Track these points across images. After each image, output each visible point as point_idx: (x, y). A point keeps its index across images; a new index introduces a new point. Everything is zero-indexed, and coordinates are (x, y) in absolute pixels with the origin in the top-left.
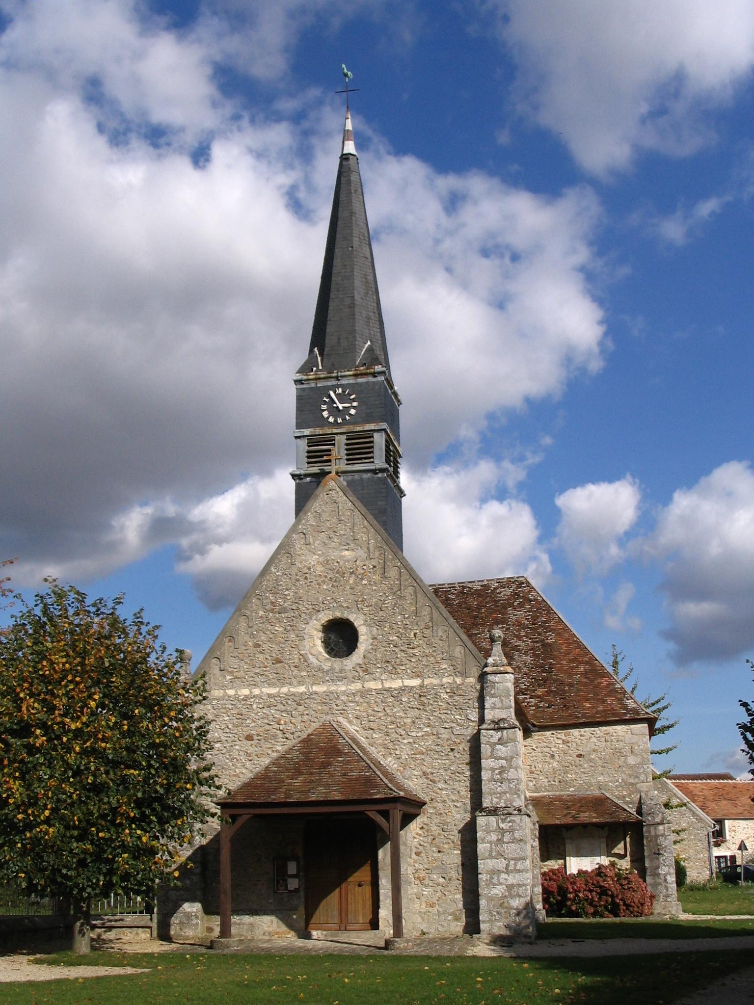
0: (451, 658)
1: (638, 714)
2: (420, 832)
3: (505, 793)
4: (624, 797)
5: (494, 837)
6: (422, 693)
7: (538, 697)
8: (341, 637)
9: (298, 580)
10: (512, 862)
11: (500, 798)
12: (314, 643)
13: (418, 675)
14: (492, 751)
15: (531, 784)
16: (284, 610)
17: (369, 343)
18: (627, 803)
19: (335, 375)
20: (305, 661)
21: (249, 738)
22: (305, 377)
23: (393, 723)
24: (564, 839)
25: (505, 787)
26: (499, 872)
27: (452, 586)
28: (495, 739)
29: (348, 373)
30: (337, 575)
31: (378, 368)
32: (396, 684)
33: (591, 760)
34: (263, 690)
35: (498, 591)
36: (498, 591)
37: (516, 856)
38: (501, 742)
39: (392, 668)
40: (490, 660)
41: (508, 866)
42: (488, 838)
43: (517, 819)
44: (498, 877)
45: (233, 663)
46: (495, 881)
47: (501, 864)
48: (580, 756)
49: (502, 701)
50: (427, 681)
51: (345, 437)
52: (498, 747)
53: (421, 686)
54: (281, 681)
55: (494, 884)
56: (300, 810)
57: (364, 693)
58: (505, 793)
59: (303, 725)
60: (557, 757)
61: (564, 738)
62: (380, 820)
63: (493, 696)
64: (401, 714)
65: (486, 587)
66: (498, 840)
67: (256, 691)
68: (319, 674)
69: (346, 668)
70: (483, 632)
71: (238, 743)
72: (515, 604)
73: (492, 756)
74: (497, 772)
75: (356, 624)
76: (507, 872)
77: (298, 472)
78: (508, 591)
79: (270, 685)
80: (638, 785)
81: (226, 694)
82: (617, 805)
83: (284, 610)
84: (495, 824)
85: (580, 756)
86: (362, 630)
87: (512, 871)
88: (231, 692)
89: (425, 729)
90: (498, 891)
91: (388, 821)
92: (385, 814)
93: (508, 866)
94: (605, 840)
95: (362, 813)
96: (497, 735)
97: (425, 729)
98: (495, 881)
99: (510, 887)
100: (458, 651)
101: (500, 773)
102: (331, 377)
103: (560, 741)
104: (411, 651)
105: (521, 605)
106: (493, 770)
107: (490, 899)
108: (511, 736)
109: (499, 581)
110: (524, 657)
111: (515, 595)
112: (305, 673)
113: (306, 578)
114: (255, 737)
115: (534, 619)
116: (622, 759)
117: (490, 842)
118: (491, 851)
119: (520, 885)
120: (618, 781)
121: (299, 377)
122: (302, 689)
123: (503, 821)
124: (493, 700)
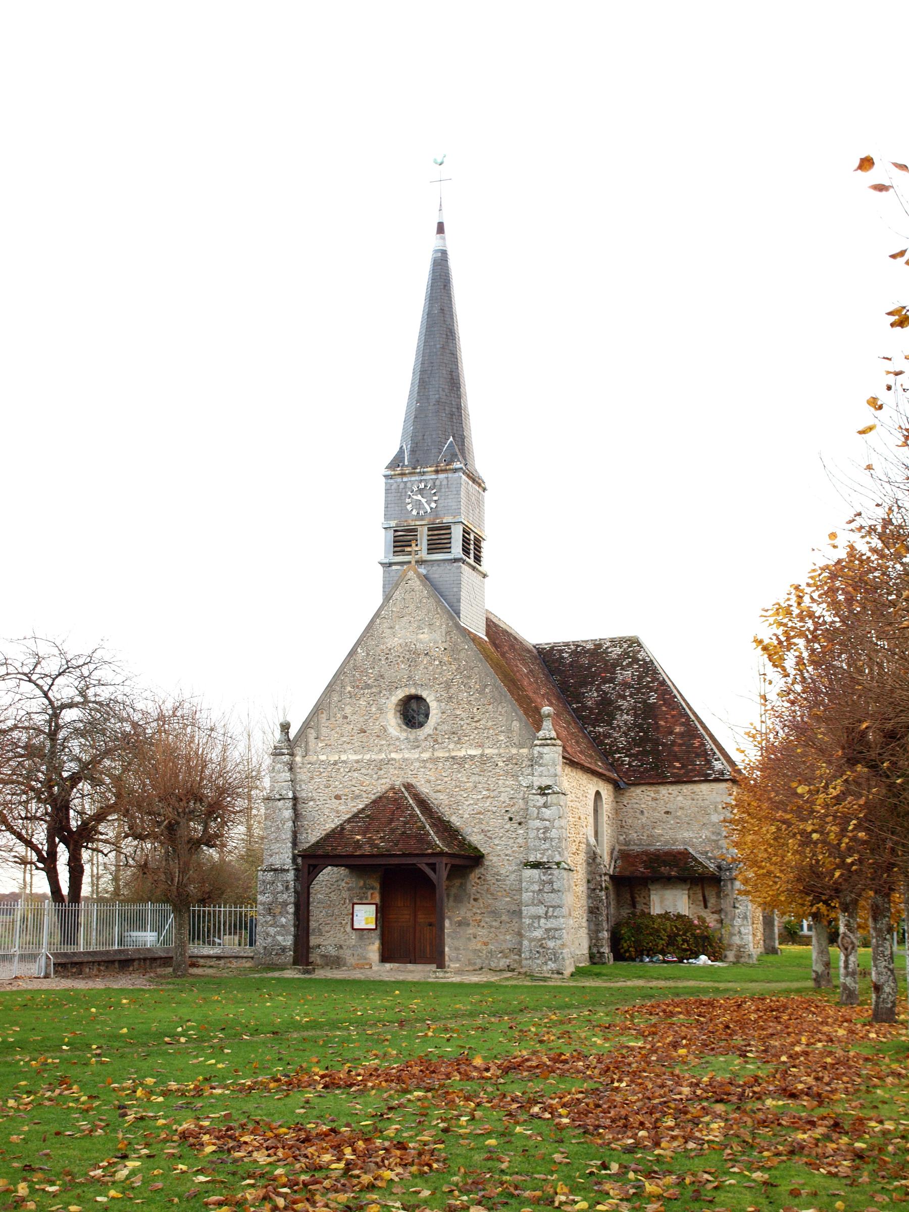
0: (510, 730)
2: (478, 881)
3: (547, 850)
4: (707, 853)
6: (484, 759)
8: (413, 712)
9: (380, 660)
10: (551, 909)
11: (543, 854)
12: (392, 722)
13: (481, 746)
14: (538, 813)
15: (621, 838)
16: (368, 686)
17: (451, 439)
18: (709, 859)
19: (418, 470)
20: (385, 731)
21: (338, 797)
22: (393, 473)
23: (456, 787)
25: (547, 845)
26: (540, 917)
28: (540, 803)
29: (429, 469)
30: (413, 656)
31: (457, 465)
32: (462, 753)
33: (677, 817)
34: (350, 756)
35: (610, 650)
36: (610, 650)
37: (554, 904)
38: (545, 806)
39: (456, 735)
40: (541, 734)
41: (547, 912)
42: (532, 888)
43: (556, 872)
44: (539, 922)
46: (536, 925)
47: (541, 910)
48: (667, 813)
50: (487, 751)
51: (426, 528)
52: (544, 810)
53: (482, 755)
54: (364, 748)
55: (535, 928)
58: (547, 850)
59: (379, 786)
60: (646, 814)
61: (653, 795)
62: (428, 870)
65: (599, 646)
66: (540, 890)
67: (344, 757)
68: (393, 744)
69: (420, 738)
70: (591, 691)
71: (329, 802)
73: (537, 818)
74: (541, 831)
75: (428, 700)
76: (547, 917)
78: (618, 651)
80: (720, 842)
81: (318, 759)
82: (696, 859)
83: (368, 686)
84: (537, 876)
85: (667, 813)
86: (433, 705)
87: (550, 917)
88: (323, 758)
89: (484, 793)
90: (538, 934)
91: (435, 872)
92: (433, 866)
93: (547, 912)
94: (686, 892)
95: (414, 864)
96: (541, 800)
97: (484, 793)
98: (536, 925)
99: (548, 930)
101: (544, 833)
102: (414, 473)
103: (650, 798)
104: (474, 724)
105: (630, 665)
106: (538, 829)
108: (555, 801)
110: (625, 717)
111: (626, 654)
112: (384, 742)
113: (387, 658)
114: (343, 797)
115: (640, 678)
116: (707, 817)
117: (533, 892)
119: (557, 930)
120: (701, 837)
122: (383, 756)
123: (544, 874)
124: (542, 768)
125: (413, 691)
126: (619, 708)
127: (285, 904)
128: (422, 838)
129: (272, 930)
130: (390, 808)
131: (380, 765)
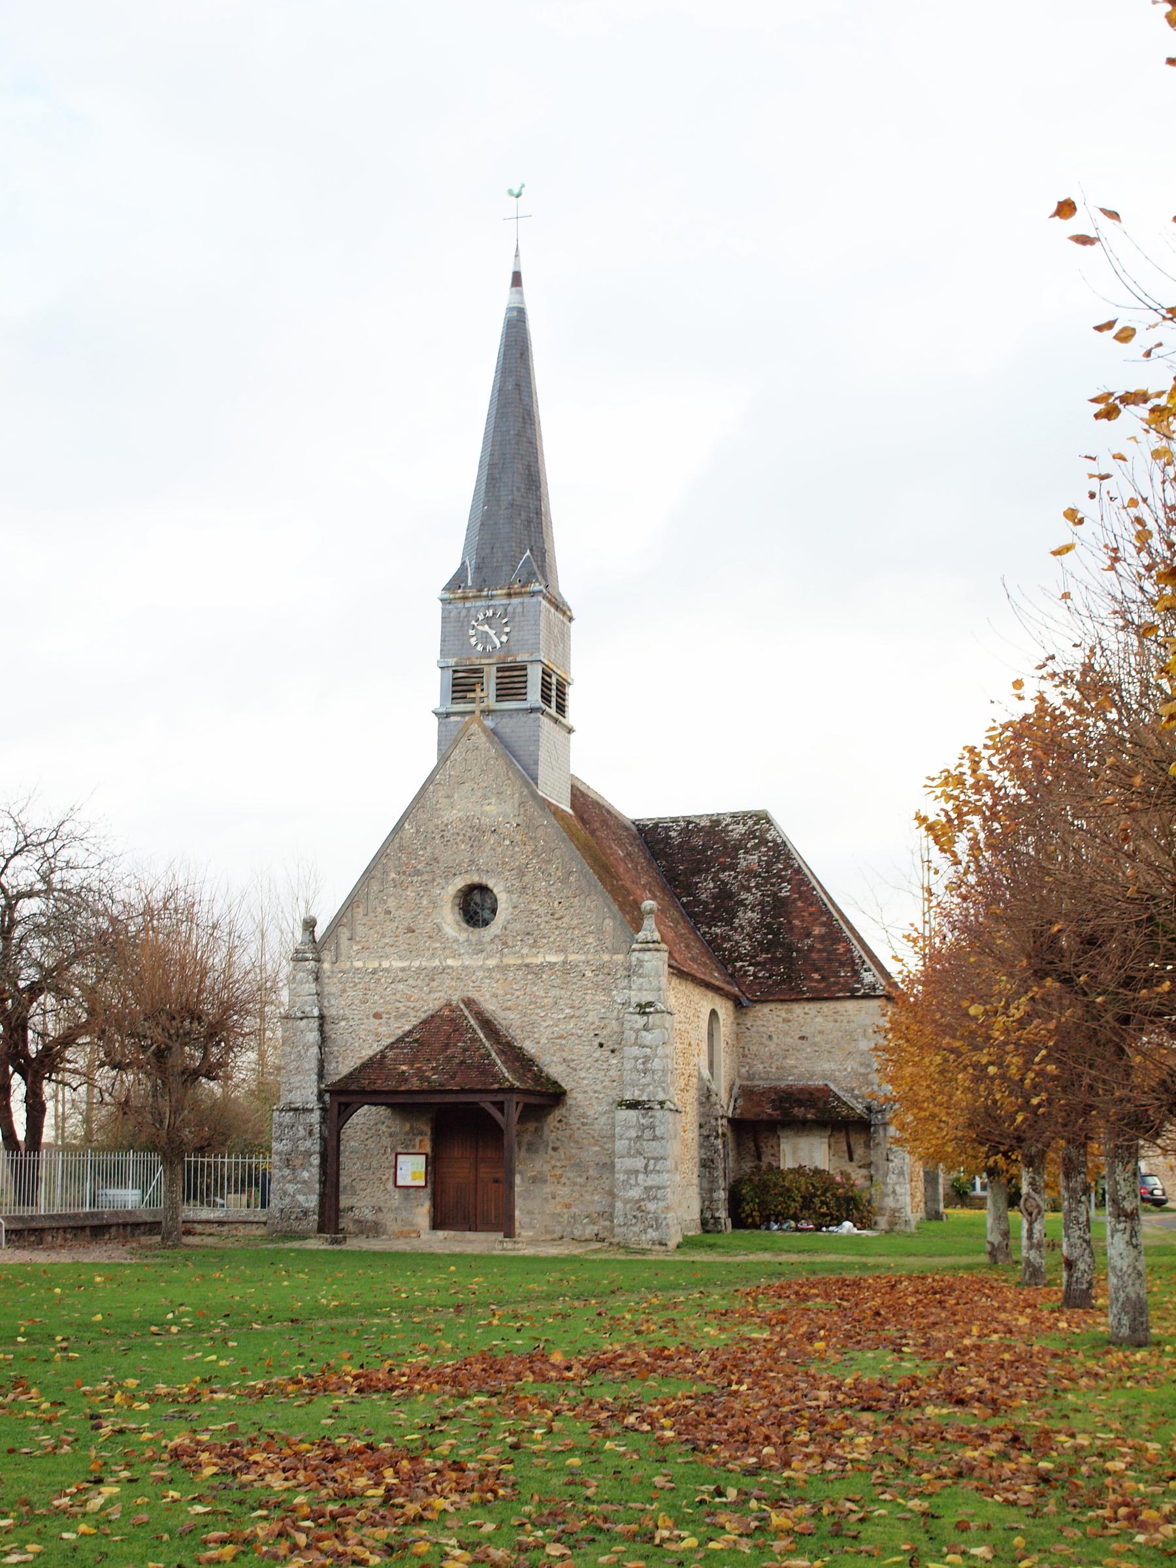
1: (875, 989)
3: (648, 1085)
5: (633, 1133)
7: (759, 964)
8: (475, 906)
10: (652, 1162)
11: (642, 1090)
12: (449, 919)
13: (563, 950)
14: (636, 1038)
16: (418, 873)
18: (856, 1097)
19: (485, 593)
21: (377, 1016)
22: (452, 596)
23: (531, 1003)
24: (779, 1138)
26: (637, 1172)
27: (675, 820)
29: (499, 592)
30: (476, 833)
33: (815, 1044)
34: (393, 963)
35: (730, 828)
36: (730, 828)
37: (656, 1154)
38: (646, 1028)
41: (646, 1166)
43: (659, 1114)
45: (360, 930)
46: (632, 1182)
47: (639, 1163)
48: (802, 1038)
49: (650, 983)
50: (572, 957)
51: (494, 668)
52: (644, 1033)
53: (564, 962)
56: (437, 1099)
57: (503, 969)
58: (648, 1085)
63: (640, 976)
64: (542, 993)
67: (386, 964)
70: (706, 880)
71: (366, 1021)
72: (749, 845)
73: (635, 1044)
74: (640, 1061)
77: (441, 710)
78: (741, 829)
79: (401, 958)
82: (838, 1098)
83: (418, 873)
85: (802, 1038)
87: (651, 1172)
88: (359, 964)
90: (635, 1193)
91: (503, 1114)
92: (500, 1106)
93: (646, 1166)
96: (641, 1021)
97: (567, 1011)
99: (647, 1189)
100: (609, 924)
101: (644, 1063)
102: (480, 596)
105: (756, 847)
106: (636, 1059)
107: (626, 1202)
108: (658, 1022)
109: (733, 816)
110: (749, 914)
111: (751, 834)
112: (438, 945)
114: (384, 1016)
117: (630, 1139)
118: (630, 1149)
119: (659, 1188)
120: (845, 1070)
121: (448, 596)
123: (644, 1116)
124: (641, 980)
125: (476, 879)
126: (741, 903)
127: (308, 1154)
128: (486, 1069)
129: (290, 1188)
130: (444, 1030)
131: (433, 975)
